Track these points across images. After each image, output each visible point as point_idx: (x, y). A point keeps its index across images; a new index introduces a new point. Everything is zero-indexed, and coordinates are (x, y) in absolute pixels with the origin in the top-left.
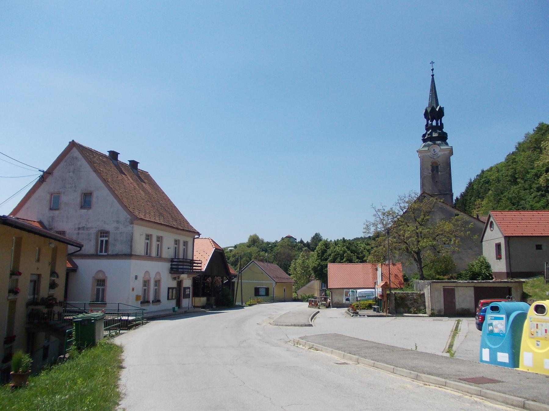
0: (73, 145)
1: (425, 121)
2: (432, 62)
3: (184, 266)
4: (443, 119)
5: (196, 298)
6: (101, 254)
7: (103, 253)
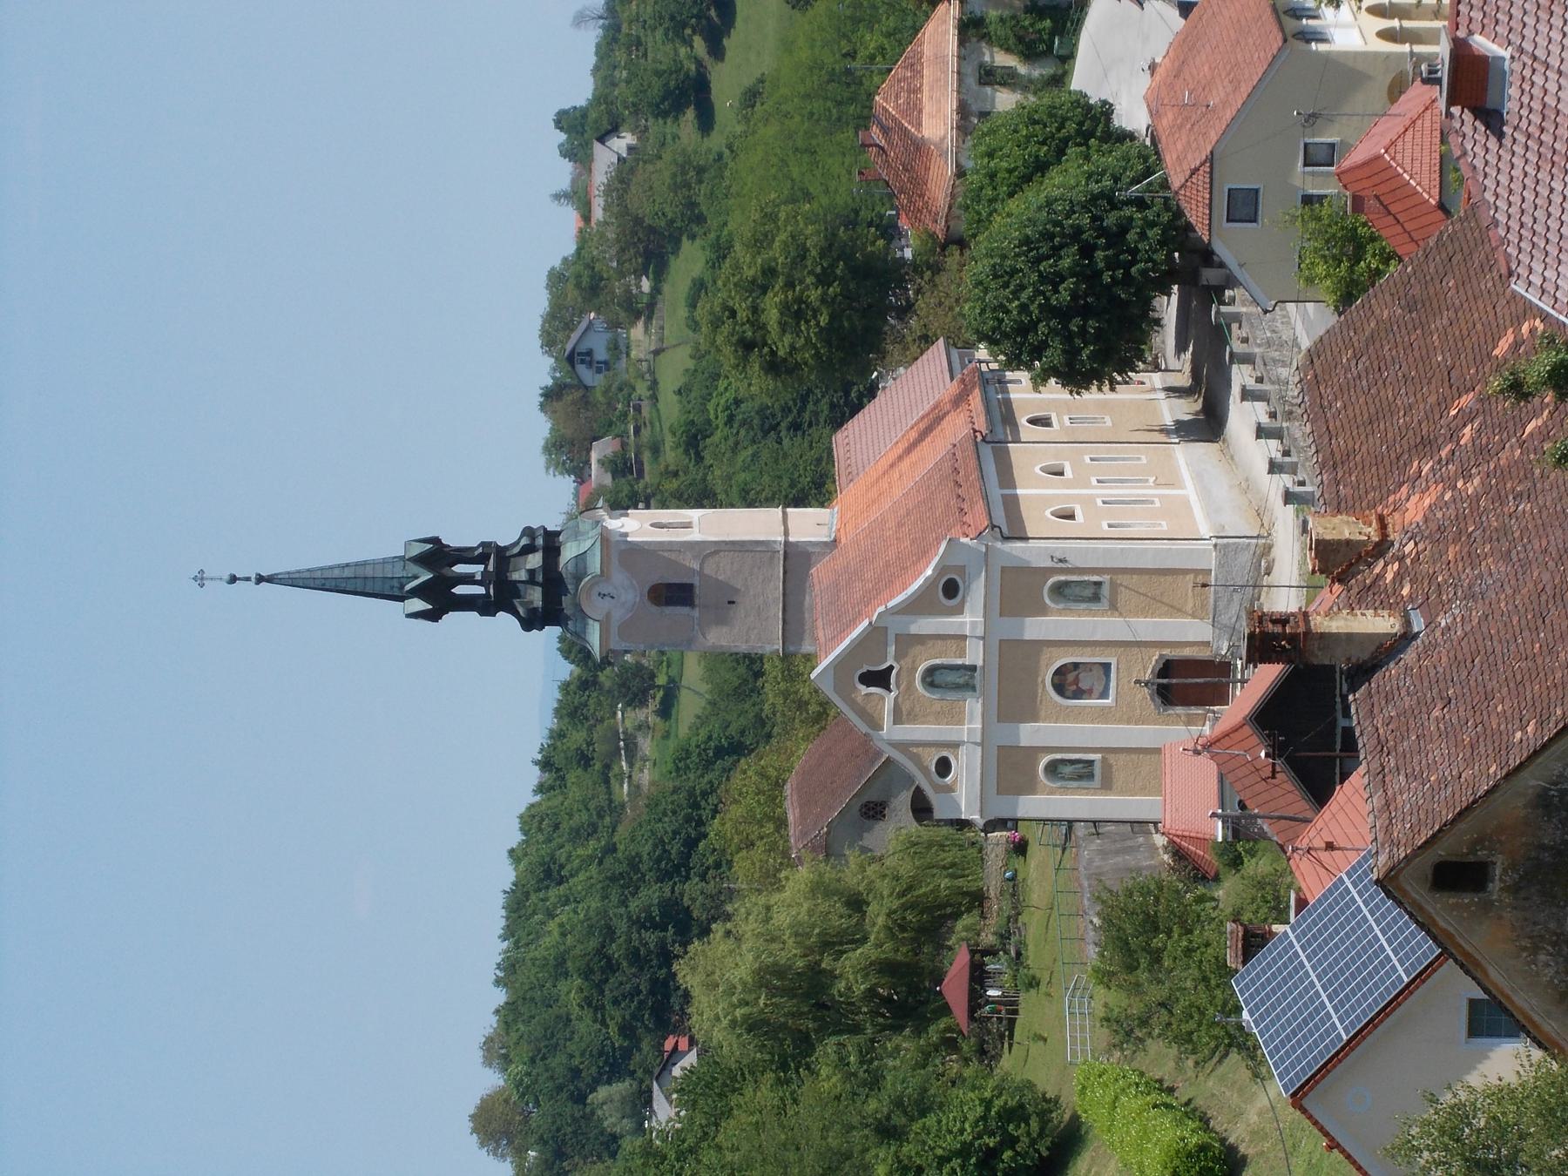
2: (195, 579)
4: (452, 540)
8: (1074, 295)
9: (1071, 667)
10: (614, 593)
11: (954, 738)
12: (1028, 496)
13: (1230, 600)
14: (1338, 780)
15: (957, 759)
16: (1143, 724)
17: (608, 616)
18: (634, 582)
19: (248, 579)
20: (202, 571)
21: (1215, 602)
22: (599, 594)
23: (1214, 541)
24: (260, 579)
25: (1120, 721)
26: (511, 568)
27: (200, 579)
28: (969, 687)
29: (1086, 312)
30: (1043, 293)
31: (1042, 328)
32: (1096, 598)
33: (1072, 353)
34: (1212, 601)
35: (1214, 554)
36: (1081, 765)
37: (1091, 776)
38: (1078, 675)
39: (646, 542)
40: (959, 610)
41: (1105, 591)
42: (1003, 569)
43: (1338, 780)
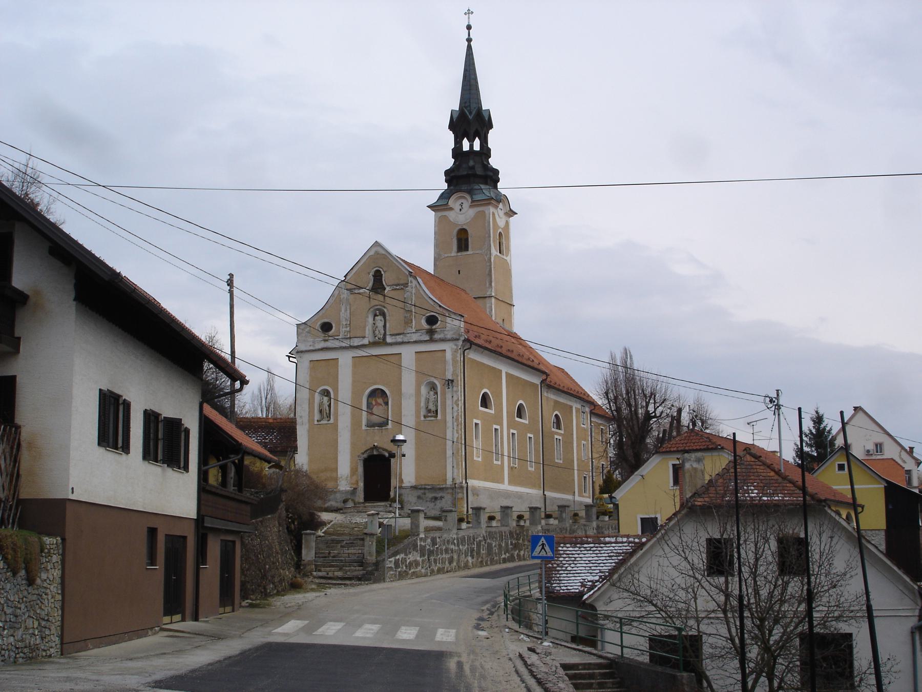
0: (489, 110)
1: (449, 138)
2: (469, 10)
3: (348, 409)
4: (491, 135)
5: (873, 609)
6: (877, 454)
7: (879, 453)
9: (386, 400)
10: (463, 211)
14: (574, 681)
22: (462, 203)
23: (465, 485)
24: (469, 40)
26: (459, 112)
27: (469, 13)
38: (381, 405)
43: (574, 681)
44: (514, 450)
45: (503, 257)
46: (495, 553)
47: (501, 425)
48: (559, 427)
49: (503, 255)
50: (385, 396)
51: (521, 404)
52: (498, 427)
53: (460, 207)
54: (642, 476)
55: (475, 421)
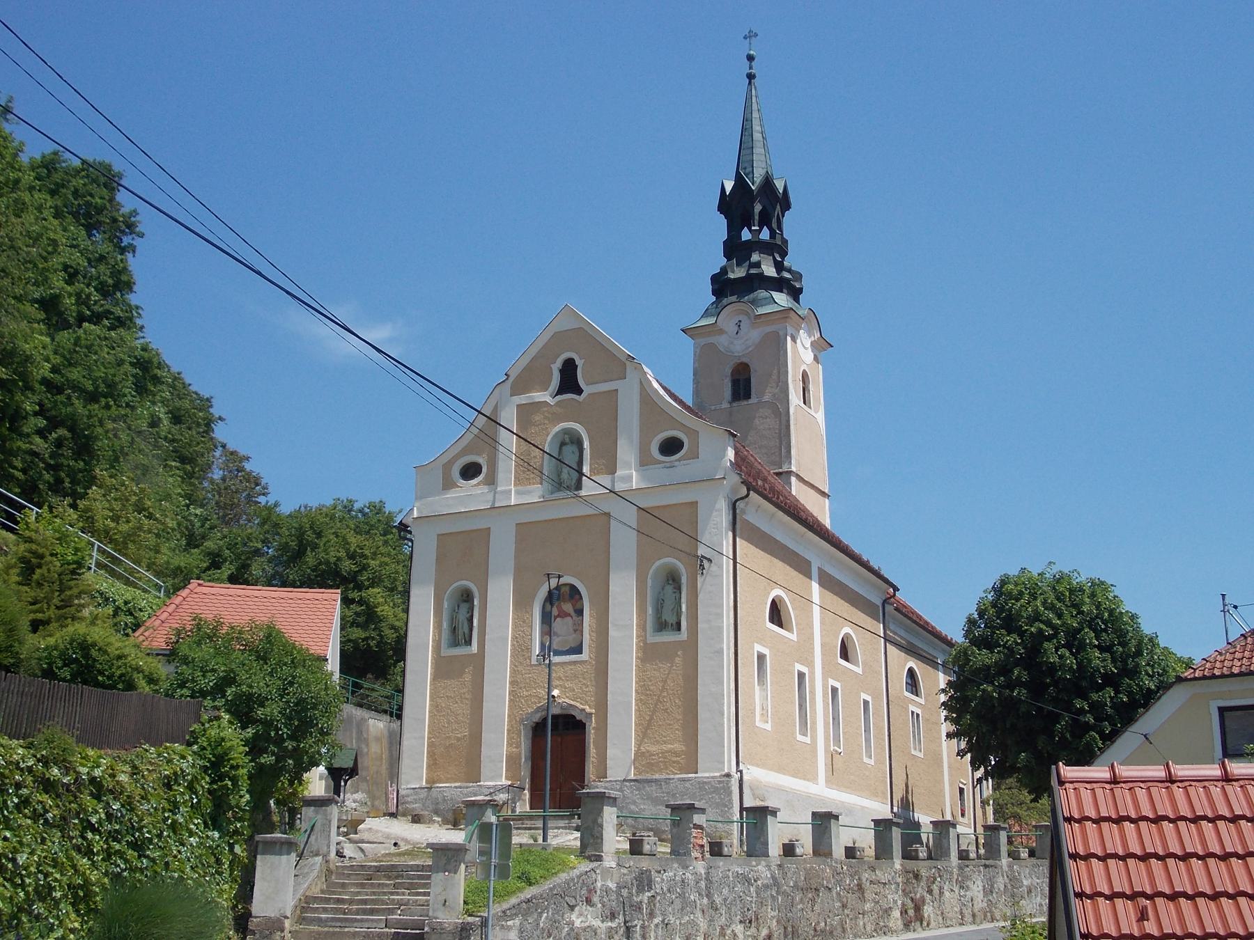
4: (789, 220)
8: (1052, 668)
10: (741, 333)
11: (501, 476)
12: (874, 795)
13: (656, 801)
15: (478, 484)
16: (510, 700)
17: (721, 332)
18: (750, 349)
19: (751, 68)
20: (756, 35)
21: (656, 781)
25: (514, 672)
27: (750, 36)
28: (559, 485)
29: (1036, 689)
30: (1055, 635)
31: (1011, 639)
32: (661, 626)
33: (986, 673)
34: (657, 776)
35: (717, 774)
36: (467, 631)
37: (455, 643)
38: (569, 615)
39: (787, 372)
40: (644, 461)
41: (668, 637)
42: (694, 505)
44: (836, 720)
45: (809, 410)
46: (50, 806)
47: (811, 665)
48: (916, 692)
49: (810, 408)
50: (577, 597)
51: (847, 636)
52: (804, 669)
53: (737, 328)
54: (1145, 736)
55: (758, 648)
